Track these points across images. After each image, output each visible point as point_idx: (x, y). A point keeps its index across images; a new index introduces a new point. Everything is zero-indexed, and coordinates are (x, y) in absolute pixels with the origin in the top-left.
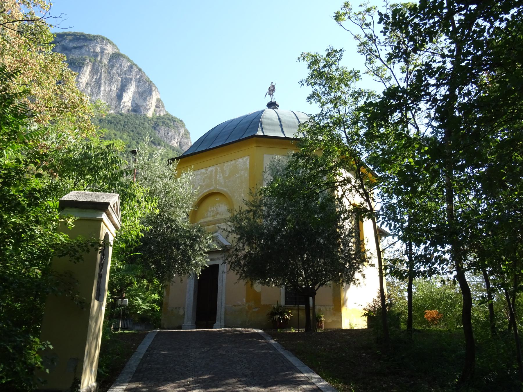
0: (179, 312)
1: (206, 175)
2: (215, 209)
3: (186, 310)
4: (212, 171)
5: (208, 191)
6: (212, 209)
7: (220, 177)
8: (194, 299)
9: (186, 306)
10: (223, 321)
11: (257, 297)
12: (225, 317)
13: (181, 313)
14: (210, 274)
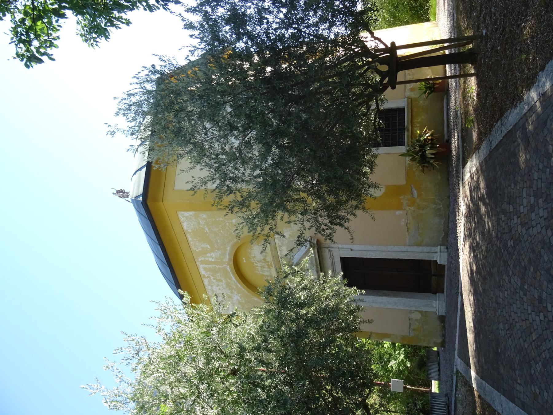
0: (416, 320)
1: (212, 278)
2: (259, 264)
3: (414, 309)
4: (205, 269)
5: (233, 274)
6: (259, 268)
7: (211, 257)
8: (394, 296)
9: (407, 308)
10: (433, 249)
11: (395, 192)
12: (428, 245)
13: (418, 316)
14: (357, 272)
